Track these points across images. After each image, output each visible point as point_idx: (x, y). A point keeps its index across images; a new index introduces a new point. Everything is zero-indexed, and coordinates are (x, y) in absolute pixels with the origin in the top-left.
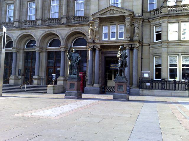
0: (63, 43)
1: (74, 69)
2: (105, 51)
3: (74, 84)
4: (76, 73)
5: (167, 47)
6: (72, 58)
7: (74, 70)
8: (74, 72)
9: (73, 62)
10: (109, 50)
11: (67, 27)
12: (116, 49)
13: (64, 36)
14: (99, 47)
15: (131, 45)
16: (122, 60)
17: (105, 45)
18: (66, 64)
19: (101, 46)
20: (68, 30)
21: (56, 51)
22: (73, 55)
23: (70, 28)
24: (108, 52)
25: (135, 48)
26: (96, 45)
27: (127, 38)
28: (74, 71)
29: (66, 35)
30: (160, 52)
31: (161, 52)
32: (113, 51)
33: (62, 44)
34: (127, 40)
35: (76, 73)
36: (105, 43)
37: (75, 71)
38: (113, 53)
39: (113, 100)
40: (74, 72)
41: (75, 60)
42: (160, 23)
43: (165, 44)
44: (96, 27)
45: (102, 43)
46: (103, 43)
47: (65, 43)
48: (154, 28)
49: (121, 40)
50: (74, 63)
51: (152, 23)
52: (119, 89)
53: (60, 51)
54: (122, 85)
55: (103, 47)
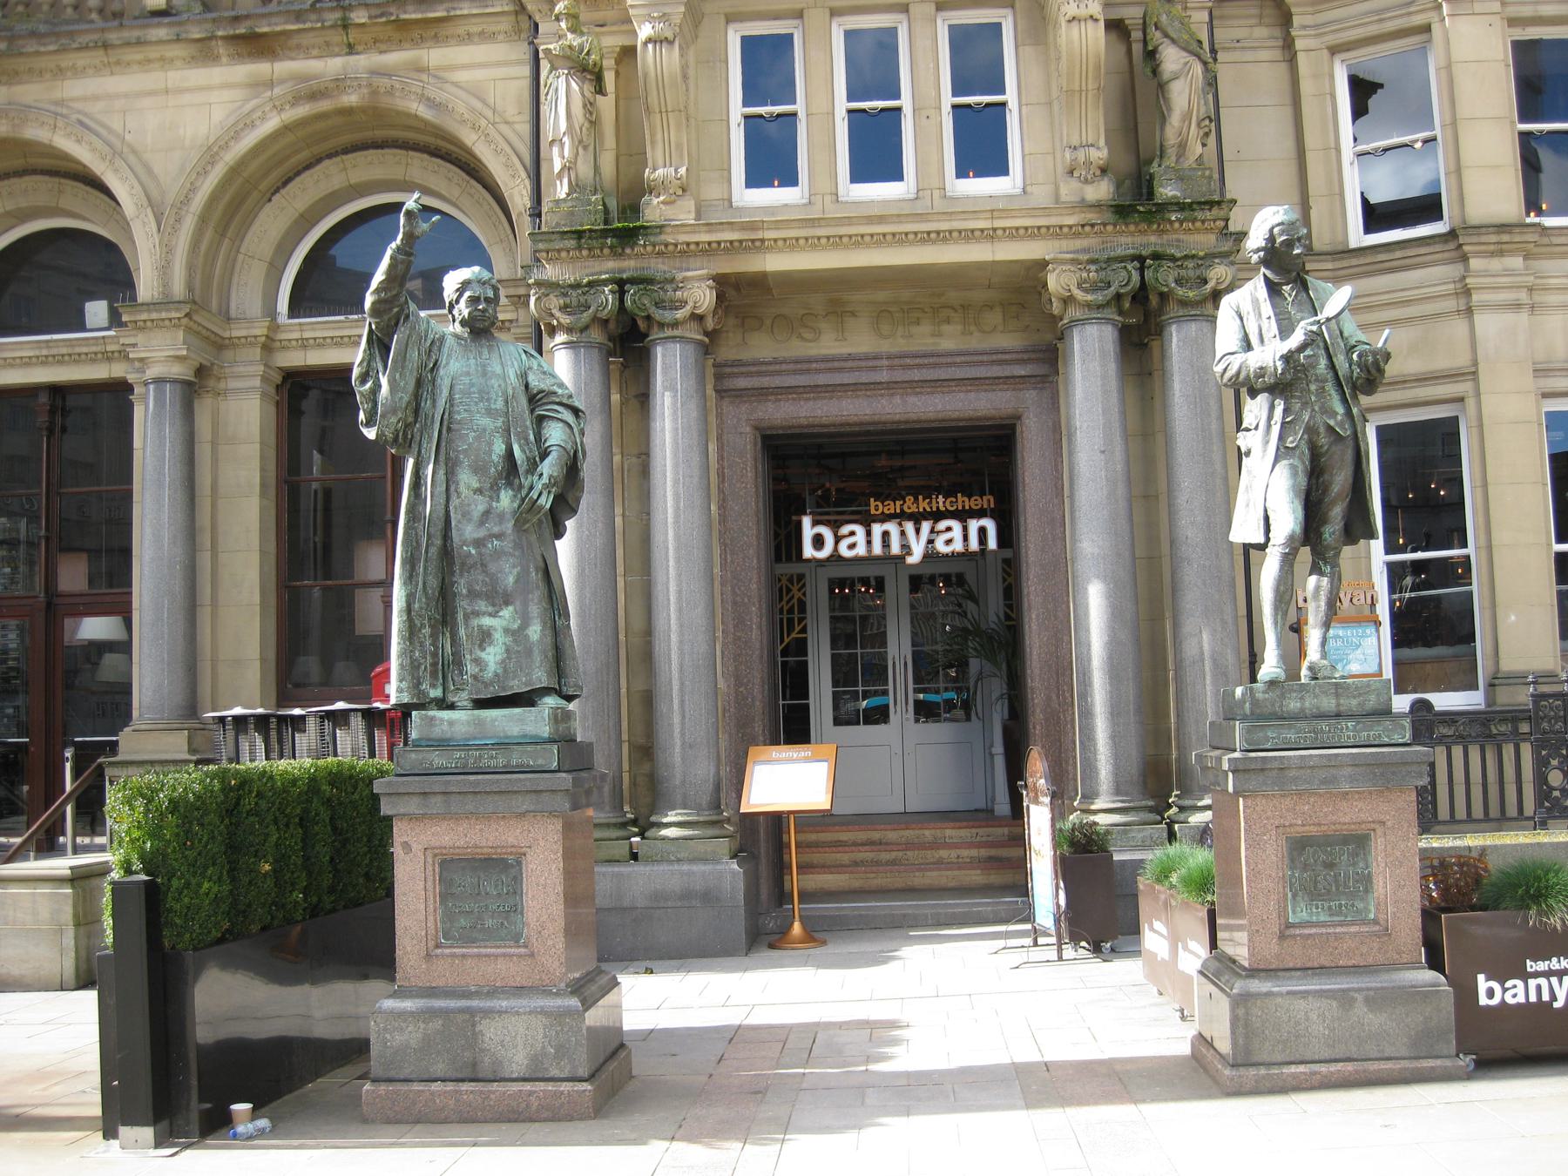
0: (154, 263)
1: (499, 598)
2: (762, 347)
3: (502, 868)
4: (540, 676)
5: (1523, 296)
6: (448, 426)
7: (500, 622)
8: (492, 656)
9: (467, 479)
10: (828, 344)
11: (214, 59)
12: (925, 328)
13: (170, 171)
14: (702, 296)
15: (621, 285)
16: (1311, 430)
17: (775, 263)
18: (205, 559)
19: (723, 284)
20: (237, 94)
21: (57, 391)
22: (455, 366)
23: (262, 68)
24: (803, 364)
25: (1184, 303)
26: (658, 267)
27: (1074, 184)
28: (485, 637)
29: (210, 156)
30: (1442, 363)
31: (1462, 360)
32: (886, 347)
33: (146, 285)
34: (1084, 205)
35: (540, 676)
36: (792, 245)
37: (517, 634)
38: (884, 376)
39: (1209, 1073)
40: (492, 656)
41: (499, 448)
42: (1418, 20)
43: (1495, 264)
44: (645, 31)
45: (733, 248)
46: (758, 246)
47: (190, 268)
48: (1332, 77)
49: (973, 209)
50: (480, 504)
51: (1309, 20)
52: (1313, 893)
53: (119, 391)
54: (1358, 842)
55: (743, 297)
